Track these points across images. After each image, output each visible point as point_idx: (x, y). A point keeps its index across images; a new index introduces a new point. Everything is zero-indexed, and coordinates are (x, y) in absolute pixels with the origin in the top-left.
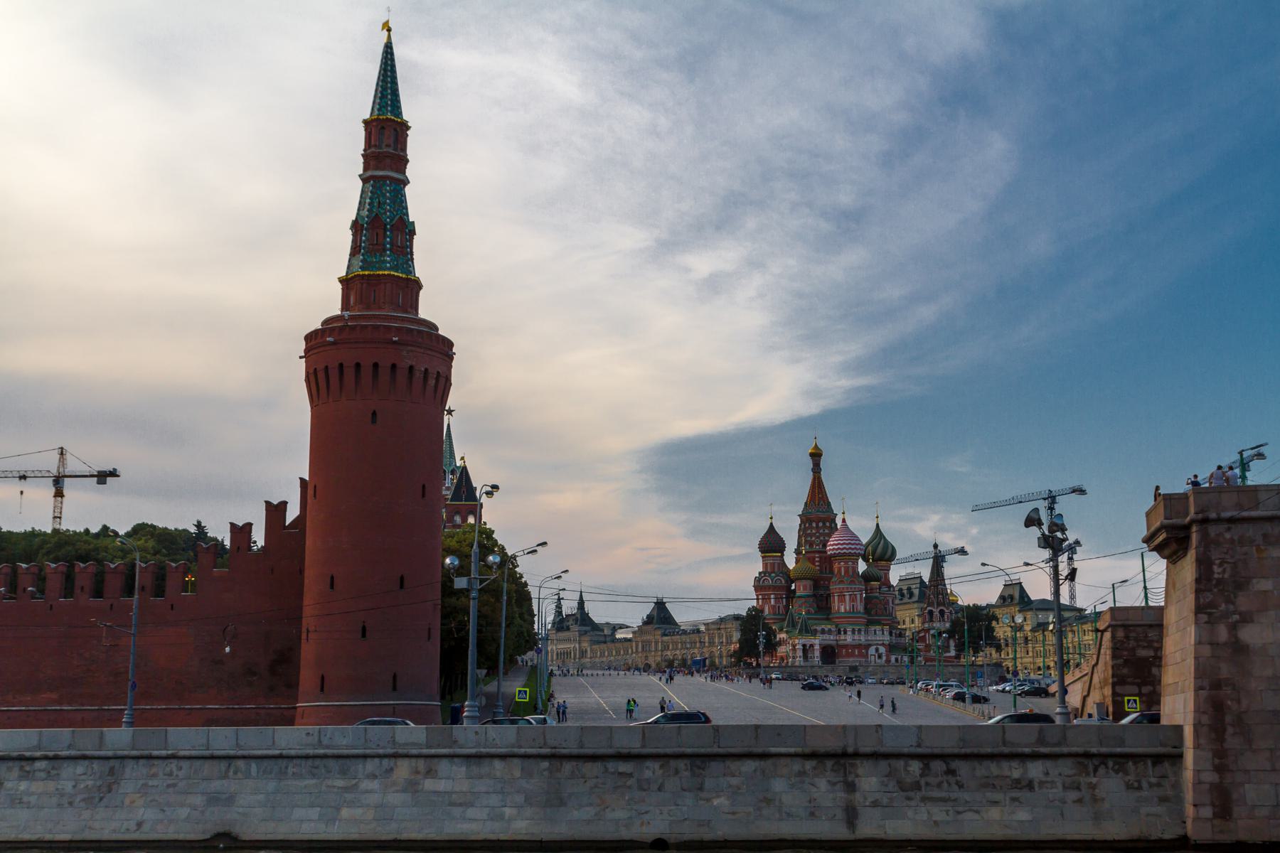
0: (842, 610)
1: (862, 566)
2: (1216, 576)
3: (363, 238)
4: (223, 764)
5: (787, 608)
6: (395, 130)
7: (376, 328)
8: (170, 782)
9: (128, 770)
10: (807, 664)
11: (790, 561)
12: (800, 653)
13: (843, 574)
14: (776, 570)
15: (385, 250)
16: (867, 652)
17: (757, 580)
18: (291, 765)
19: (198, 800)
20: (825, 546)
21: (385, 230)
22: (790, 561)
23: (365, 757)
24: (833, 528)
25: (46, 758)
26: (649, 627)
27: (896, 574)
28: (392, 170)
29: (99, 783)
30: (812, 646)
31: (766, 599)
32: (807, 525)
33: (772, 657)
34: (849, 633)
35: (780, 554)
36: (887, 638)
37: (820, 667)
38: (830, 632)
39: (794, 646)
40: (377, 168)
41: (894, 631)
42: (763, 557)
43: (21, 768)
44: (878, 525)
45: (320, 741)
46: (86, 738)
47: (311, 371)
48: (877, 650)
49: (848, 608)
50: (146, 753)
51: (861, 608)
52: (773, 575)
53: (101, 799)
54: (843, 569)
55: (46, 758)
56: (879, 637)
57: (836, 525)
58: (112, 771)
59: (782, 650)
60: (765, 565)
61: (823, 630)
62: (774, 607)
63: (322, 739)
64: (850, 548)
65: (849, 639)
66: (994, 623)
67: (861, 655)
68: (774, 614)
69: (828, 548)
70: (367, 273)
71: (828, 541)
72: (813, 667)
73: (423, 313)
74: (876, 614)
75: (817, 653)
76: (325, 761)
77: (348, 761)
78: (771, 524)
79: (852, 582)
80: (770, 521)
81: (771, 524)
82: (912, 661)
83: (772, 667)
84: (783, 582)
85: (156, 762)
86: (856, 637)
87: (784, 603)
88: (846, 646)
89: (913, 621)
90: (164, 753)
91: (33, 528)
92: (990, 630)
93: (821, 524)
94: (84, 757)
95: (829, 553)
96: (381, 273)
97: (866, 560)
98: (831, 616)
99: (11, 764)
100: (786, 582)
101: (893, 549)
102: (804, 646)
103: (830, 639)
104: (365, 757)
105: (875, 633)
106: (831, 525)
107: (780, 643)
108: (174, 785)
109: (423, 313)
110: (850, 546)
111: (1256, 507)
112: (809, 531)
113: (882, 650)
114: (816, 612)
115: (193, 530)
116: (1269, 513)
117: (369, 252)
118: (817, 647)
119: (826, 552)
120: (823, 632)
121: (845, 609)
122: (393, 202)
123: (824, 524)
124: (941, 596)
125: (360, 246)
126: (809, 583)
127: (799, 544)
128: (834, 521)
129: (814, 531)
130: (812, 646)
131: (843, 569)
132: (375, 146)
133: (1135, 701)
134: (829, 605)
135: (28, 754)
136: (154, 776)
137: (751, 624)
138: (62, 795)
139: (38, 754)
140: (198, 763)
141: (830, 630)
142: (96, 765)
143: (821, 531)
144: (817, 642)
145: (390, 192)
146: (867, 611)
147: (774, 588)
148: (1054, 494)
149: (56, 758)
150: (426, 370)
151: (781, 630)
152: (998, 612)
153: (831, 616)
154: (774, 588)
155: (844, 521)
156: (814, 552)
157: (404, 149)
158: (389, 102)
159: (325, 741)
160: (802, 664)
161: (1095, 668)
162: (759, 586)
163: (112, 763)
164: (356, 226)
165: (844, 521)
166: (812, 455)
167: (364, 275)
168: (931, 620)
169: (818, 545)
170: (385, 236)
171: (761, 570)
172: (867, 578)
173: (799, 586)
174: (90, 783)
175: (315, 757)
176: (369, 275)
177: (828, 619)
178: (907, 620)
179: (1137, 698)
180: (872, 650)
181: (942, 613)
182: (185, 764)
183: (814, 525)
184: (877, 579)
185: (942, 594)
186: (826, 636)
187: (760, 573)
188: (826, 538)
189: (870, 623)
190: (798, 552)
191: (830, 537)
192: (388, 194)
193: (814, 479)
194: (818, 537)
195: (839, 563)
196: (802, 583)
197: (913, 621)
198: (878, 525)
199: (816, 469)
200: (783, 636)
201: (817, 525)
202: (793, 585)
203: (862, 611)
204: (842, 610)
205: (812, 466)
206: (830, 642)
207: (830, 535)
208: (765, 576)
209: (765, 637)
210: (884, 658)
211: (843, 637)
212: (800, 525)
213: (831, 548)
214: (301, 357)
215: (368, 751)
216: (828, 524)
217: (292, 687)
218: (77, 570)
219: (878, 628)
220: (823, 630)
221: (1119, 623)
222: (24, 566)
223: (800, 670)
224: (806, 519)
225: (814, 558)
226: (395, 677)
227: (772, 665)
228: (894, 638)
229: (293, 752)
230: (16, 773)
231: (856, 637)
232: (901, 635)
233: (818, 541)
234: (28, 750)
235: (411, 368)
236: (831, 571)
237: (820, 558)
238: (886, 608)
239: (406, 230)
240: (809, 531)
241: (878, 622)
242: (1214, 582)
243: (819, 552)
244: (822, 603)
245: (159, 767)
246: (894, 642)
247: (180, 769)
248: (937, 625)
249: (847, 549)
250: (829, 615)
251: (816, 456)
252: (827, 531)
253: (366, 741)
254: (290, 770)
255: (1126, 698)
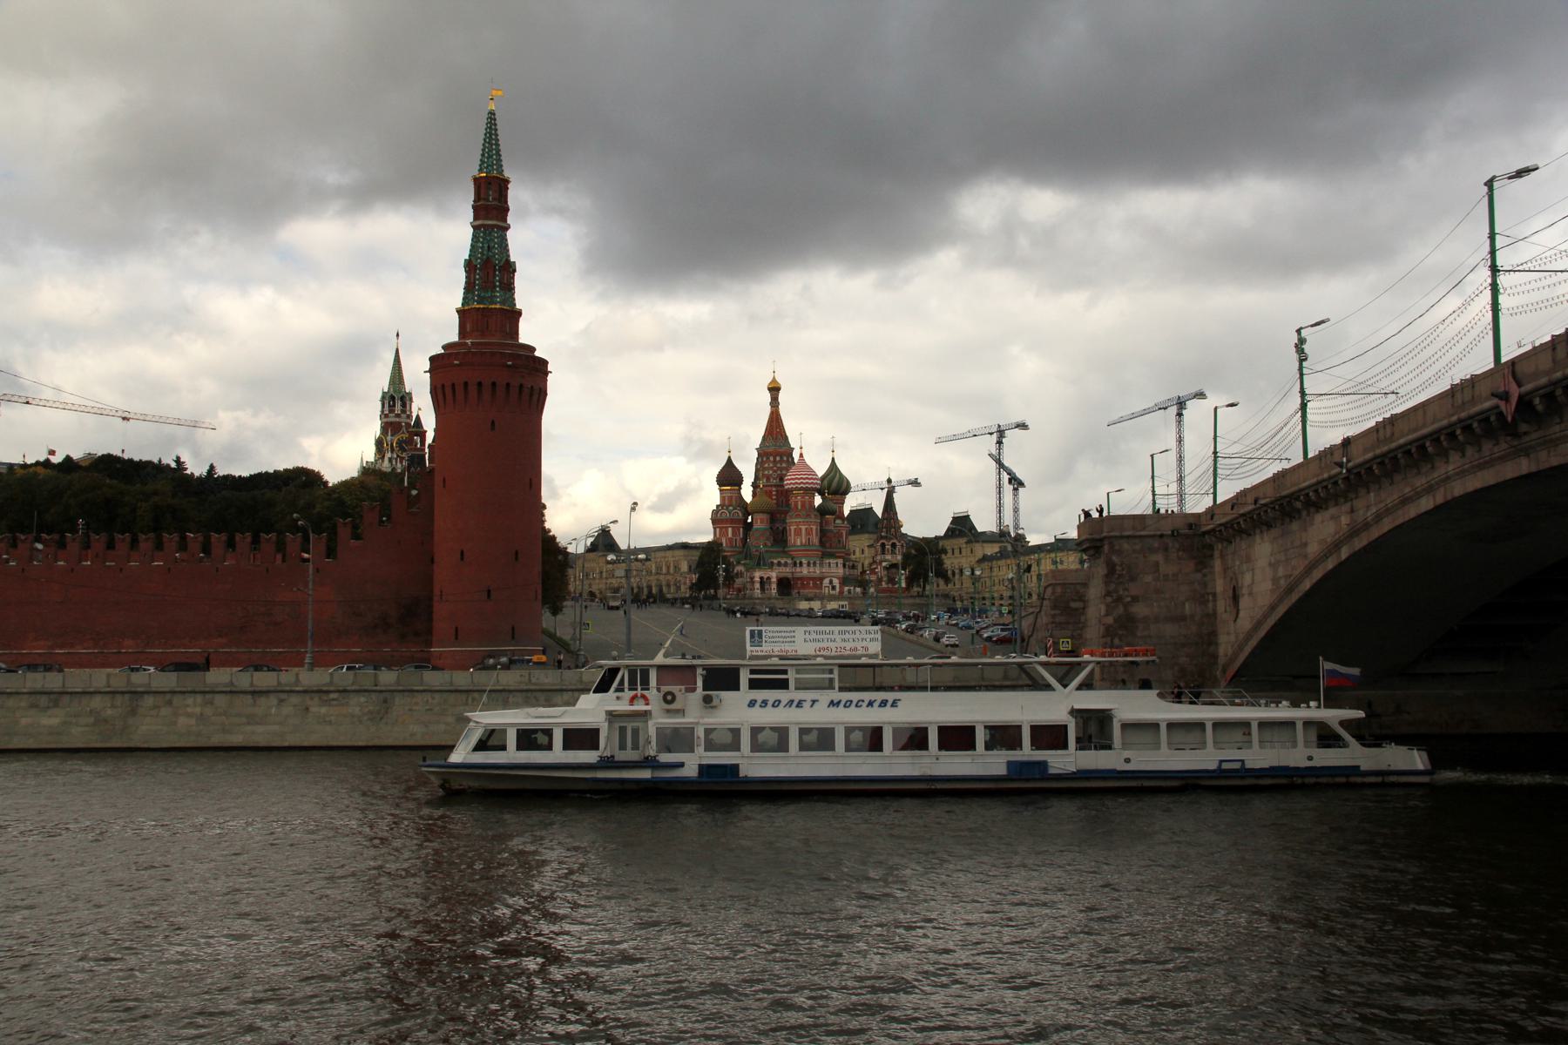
0: (799, 543)
1: (818, 500)
2: (1117, 572)
3: (477, 277)
4: (464, 696)
5: (744, 540)
6: (500, 185)
7: (493, 354)
8: (427, 707)
9: (397, 700)
10: (764, 596)
11: (747, 493)
12: (757, 586)
13: (799, 507)
14: (734, 503)
15: (495, 287)
16: (821, 583)
17: (715, 513)
18: (511, 696)
19: (450, 719)
20: (782, 479)
21: (495, 270)
22: (747, 493)
23: (562, 690)
24: (791, 462)
25: (339, 691)
26: (592, 555)
27: (851, 503)
28: (497, 220)
29: (377, 708)
30: (769, 578)
31: (724, 532)
32: (765, 459)
33: (729, 588)
34: (805, 565)
35: (737, 488)
36: (841, 571)
37: (777, 599)
38: (786, 564)
39: (752, 578)
40: (487, 218)
41: (847, 563)
42: (720, 490)
43: (320, 698)
44: (833, 459)
45: (530, 680)
46: (366, 676)
47: (439, 386)
48: (831, 582)
49: (804, 541)
50: (409, 688)
51: (816, 540)
52: (731, 508)
53: (381, 719)
54: (799, 503)
55: (339, 691)
56: (834, 570)
57: (793, 459)
58: (385, 701)
59: (739, 582)
60: (722, 499)
61: (779, 562)
62: (730, 540)
63: (532, 679)
64: (807, 483)
65: (805, 571)
66: (943, 556)
67: (815, 586)
68: (732, 547)
69: (785, 482)
70: (482, 306)
71: (785, 475)
72: (769, 599)
73: (524, 338)
74: (831, 548)
75: (774, 586)
76: (535, 694)
77: (549, 693)
78: (729, 457)
79: (808, 516)
80: (728, 455)
81: (729, 457)
82: (864, 593)
83: (730, 599)
84: (740, 515)
85: (416, 694)
86: (812, 569)
87: (741, 536)
88: (802, 579)
89: (863, 552)
90: (421, 688)
91: (160, 461)
92: (940, 563)
93: (778, 458)
94: (366, 691)
95: (786, 487)
96: (493, 306)
97: (821, 493)
98: (786, 550)
99: (313, 695)
100: (744, 515)
101: (848, 482)
102: (761, 578)
103: (786, 571)
104: (562, 690)
105: (830, 565)
106: (788, 460)
107: (740, 575)
108: (431, 710)
109: (524, 338)
110: (807, 481)
111: (1144, 529)
112: (766, 465)
113: (836, 582)
114: (772, 545)
115: (173, 465)
116: (1152, 533)
117: (483, 288)
118: (774, 580)
119: (783, 486)
120: (779, 564)
121: (801, 542)
122: (500, 246)
123: (781, 457)
124: (893, 530)
125: (475, 282)
126: (764, 516)
127: (757, 478)
128: (790, 455)
129: (771, 465)
130: (769, 578)
131: (799, 503)
132: (484, 199)
133: (1068, 642)
134: (785, 538)
135: (325, 689)
136: (416, 704)
137: (706, 557)
138: (353, 716)
139: (332, 688)
140: (445, 695)
141: (786, 563)
142: (374, 696)
143: (779, 465)
144: (774, 575)
145: (497, 238)
146: (822, 543)
147: (732, 521)
148: (1002, 428)
149: (345, 691)
150: (532, 387)
151: (739, 563)
152: (948, 544)
153: (786, 550)
154: (732, 521)
155: (801, 455)
156: (771, 486)
157: (506, 202)
158: (495, 162)
159: (533, 680)
160: (760, 596)
161: (1039, 616)
162: (717, 519)
163: (384, 694)
164: (469, 266)
165: (801, 455)
166: (770, 389)
167: (479, 308)
168: (883, 553)
169: (774, 479)
170: (495, 276)
171: (719, 503)
172: (822, 511)
173: (757, 519)
174: (371, 708)
175: (527, 691)
176: (484, 308)
177: (784, 552)
178: (857, 550)
179: (1069, 640)
180: (826, 582)
181: (894, 545)
182: (437, 696)
183: (772, 459)
184: (833, 513)
185: (895, 528)
186: (782, 569)
187: (718, 506)
188: (784, 472)
189: (825, 555)
190: (755, 485)
191: (788, 470)
192: (496, 240)
193: (772, 413)
194: (775, 471)
195: (796, 497)
196: (759, 516)
197: (863, 552)
198: (833, 459)
199: (775, 402)
200: (739, 568)
201: (775, 459)
202: (750, 517)
203: (817, 543)
204: (799, 543)
205: (770, 400)
206: (786, 575)
207: (787, 470)
208: (722, 508)
209: (725, 570)
210: (838, 589)
211: (798, 569)
212: (757, 459)
213: (789, 482)
214: (425, 372)
215: (564, 687)
216: (785, 459)
217: (426, 635)
218: (213, 540)
219: (832, 561)
220: (779, 562)
221: (1058, 582)
222: (192, 535)
223: (757, 601)
224: (763, 454)
225: (771, 492)
226: (513, 629)
227: (728, 597)
228: (847, 570)
229: (512, 688)
230: (316, 699)
231: (812, 569)
232: (853, 567)
233: (775, 475)
234: (324, 685)
235: (521, 386)
236: (788, 505)
237: (777, 491)
238: (839, 541)
239: (509, 269)
240: (766, 465)
241: (832, 556)
242: (1117, 576)
243: (775, 486)
244: (779, 538)
245: (419, 698)
246: (847, 573)
247: (433, 698)
248: (889, 557)
249: (804, 484)
250: (784, 548)
251: (774, 390)
252: (784, 465)
253: (562, 680)
254: (511, 700)
255: (1062, 640)
